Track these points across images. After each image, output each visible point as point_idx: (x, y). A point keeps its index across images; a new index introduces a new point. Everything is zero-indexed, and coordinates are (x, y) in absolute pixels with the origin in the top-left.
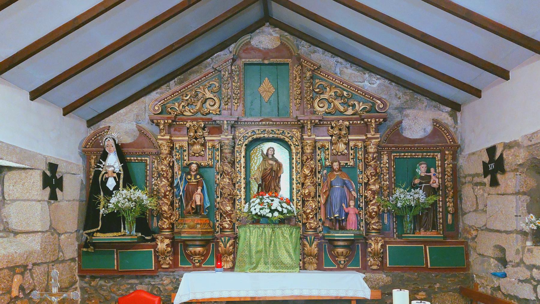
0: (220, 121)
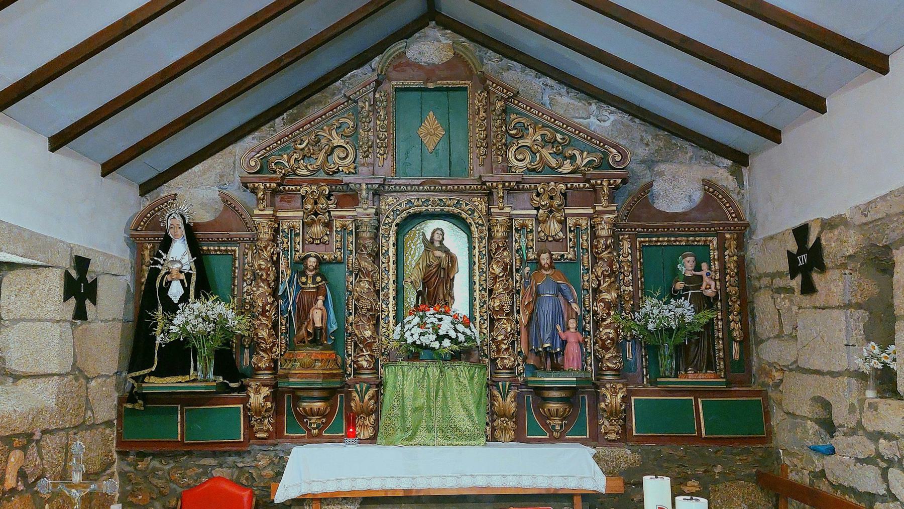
0: (355, 184)
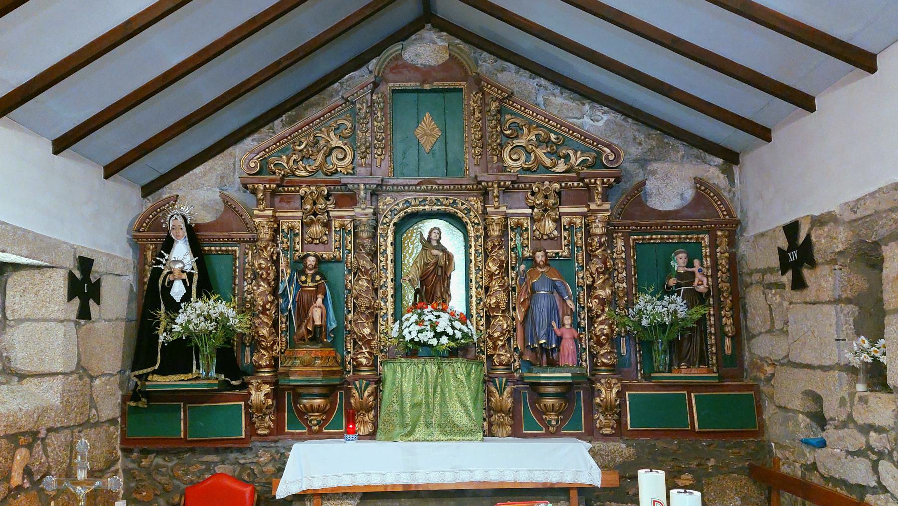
0: (353, 184)
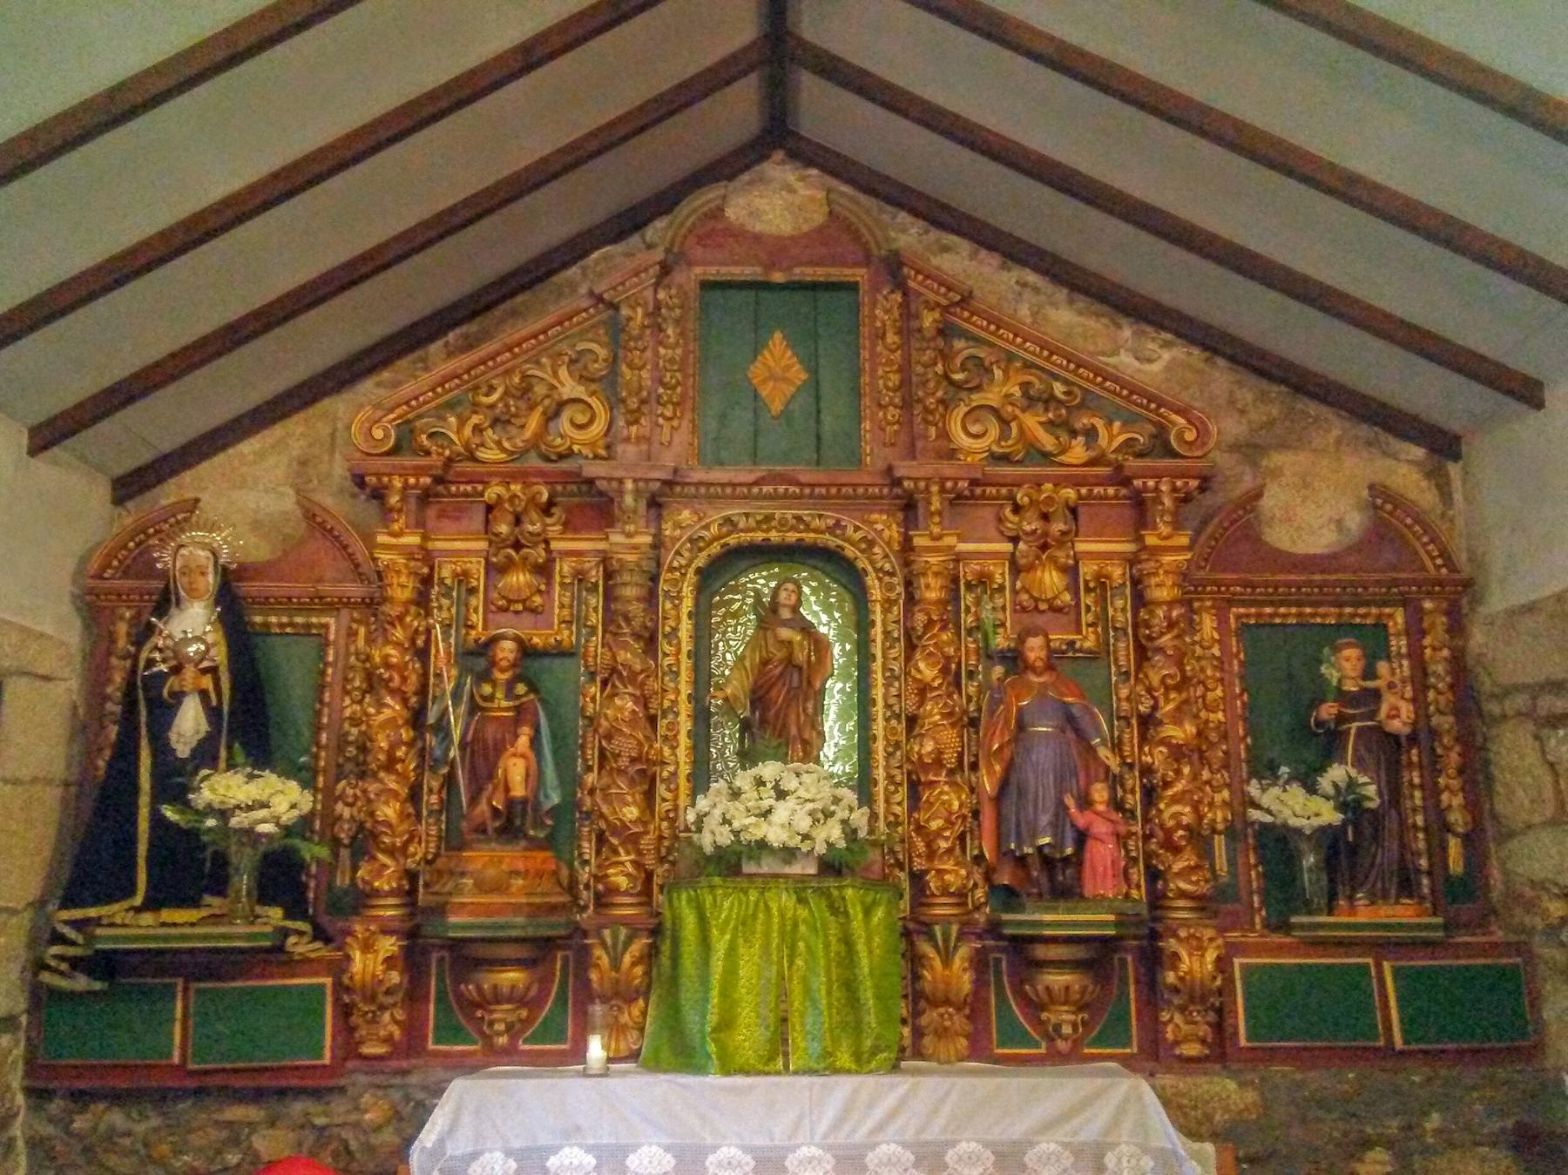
0: (610, 479)
